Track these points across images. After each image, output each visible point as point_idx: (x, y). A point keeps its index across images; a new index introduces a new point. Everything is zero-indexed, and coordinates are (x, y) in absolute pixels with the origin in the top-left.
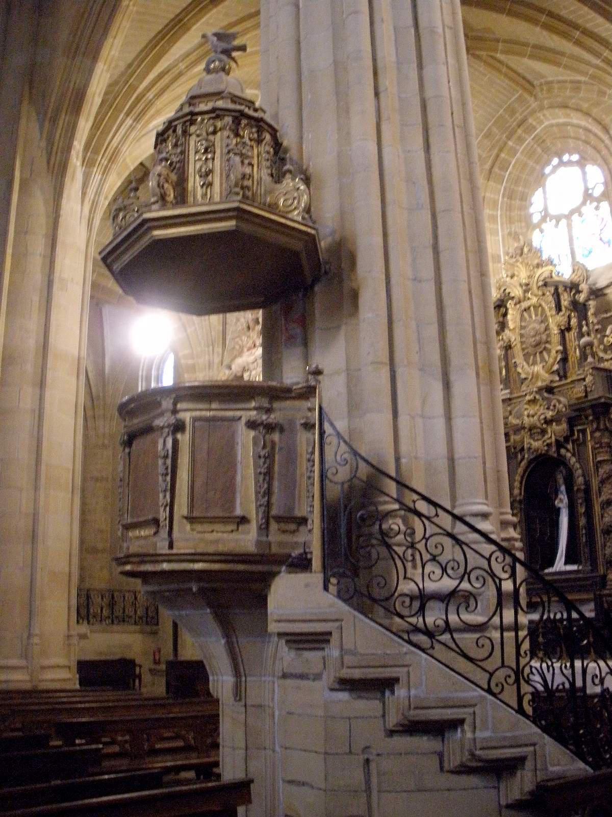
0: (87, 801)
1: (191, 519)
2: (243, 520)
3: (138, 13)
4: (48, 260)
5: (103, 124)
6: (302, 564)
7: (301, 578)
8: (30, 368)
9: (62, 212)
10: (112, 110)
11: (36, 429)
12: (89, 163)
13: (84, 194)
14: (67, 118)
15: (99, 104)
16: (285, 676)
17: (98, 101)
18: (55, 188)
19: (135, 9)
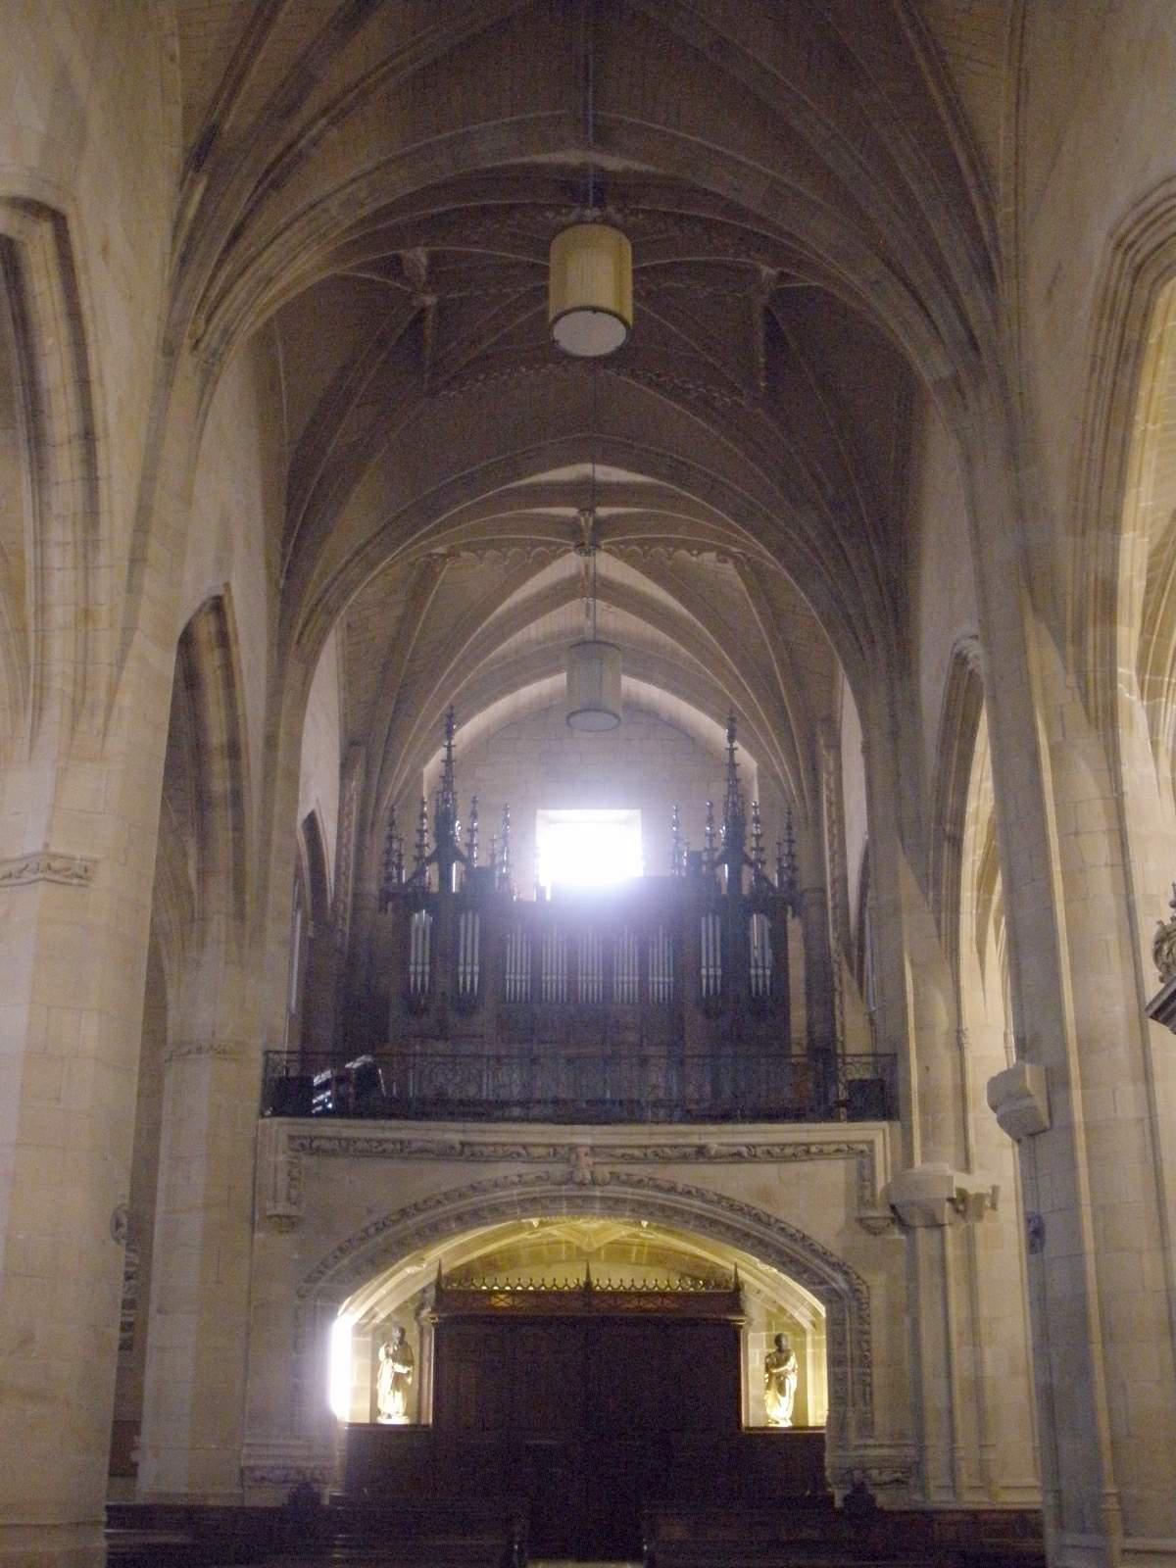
3: (1165, 429)
4: (1120, 871)
5: (1160, 617)
9: (1126, 788)
10: (1166, 594)
11: (1149, 1151)
12: (1151, 692)
13: (1155, 744)
14: (1098, 633)
15: (1143, 590)
17: (1140, 586)
18: (1106, 748)
19: (1158, 426)
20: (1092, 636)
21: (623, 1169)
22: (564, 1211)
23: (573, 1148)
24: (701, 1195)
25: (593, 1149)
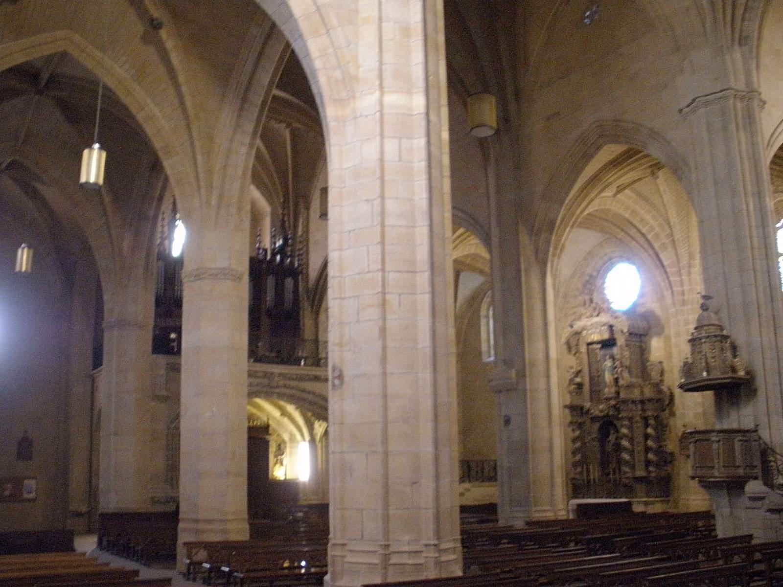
0: (581, 567)
1: (724, 467)
2: (738, 467)
6: (756, 478)
7: (756, 482)
8: (541, 368)
16: (747, 508)
20: (543, 236)
21: (288, 382)
22: (285, 399)
23: (272, 373)
24: (314, 393)
25: (280, 375)
